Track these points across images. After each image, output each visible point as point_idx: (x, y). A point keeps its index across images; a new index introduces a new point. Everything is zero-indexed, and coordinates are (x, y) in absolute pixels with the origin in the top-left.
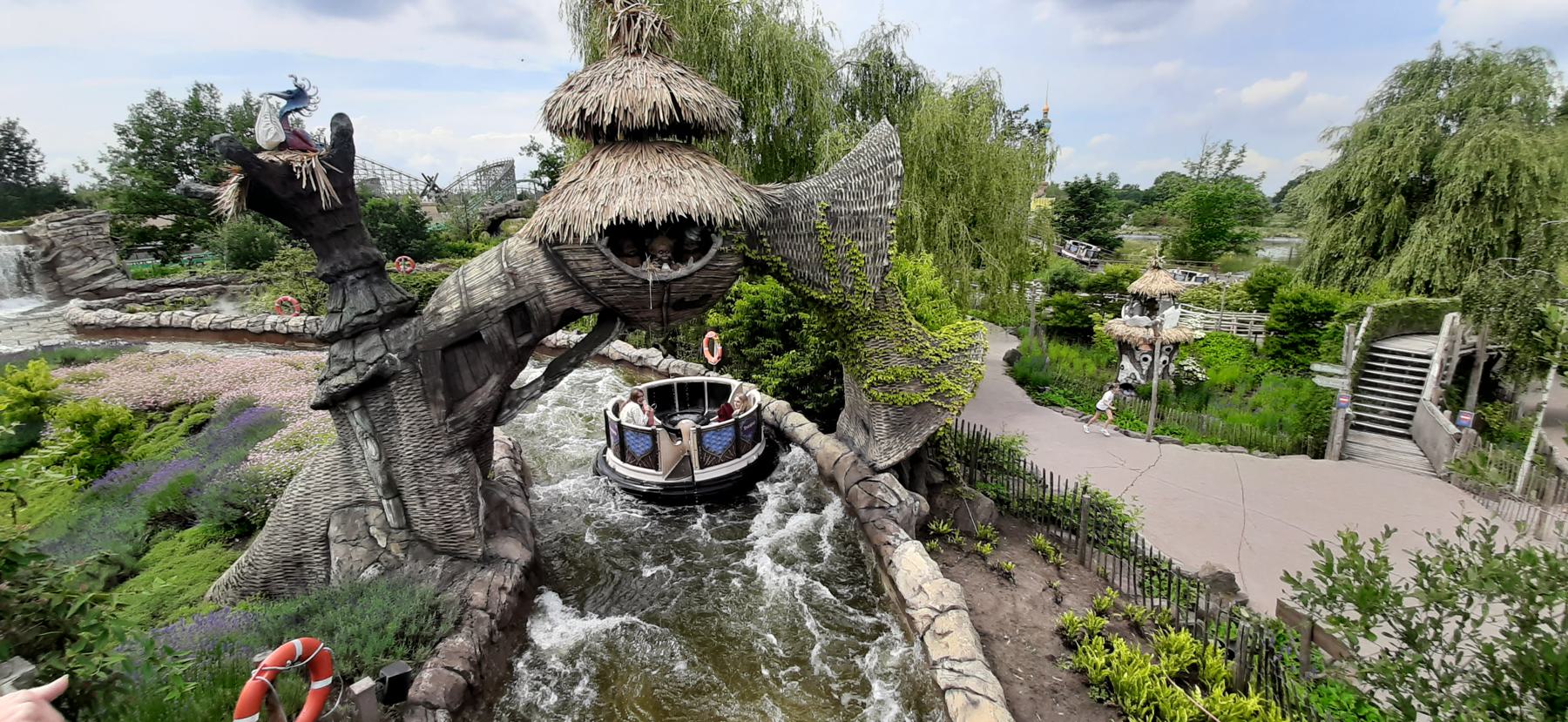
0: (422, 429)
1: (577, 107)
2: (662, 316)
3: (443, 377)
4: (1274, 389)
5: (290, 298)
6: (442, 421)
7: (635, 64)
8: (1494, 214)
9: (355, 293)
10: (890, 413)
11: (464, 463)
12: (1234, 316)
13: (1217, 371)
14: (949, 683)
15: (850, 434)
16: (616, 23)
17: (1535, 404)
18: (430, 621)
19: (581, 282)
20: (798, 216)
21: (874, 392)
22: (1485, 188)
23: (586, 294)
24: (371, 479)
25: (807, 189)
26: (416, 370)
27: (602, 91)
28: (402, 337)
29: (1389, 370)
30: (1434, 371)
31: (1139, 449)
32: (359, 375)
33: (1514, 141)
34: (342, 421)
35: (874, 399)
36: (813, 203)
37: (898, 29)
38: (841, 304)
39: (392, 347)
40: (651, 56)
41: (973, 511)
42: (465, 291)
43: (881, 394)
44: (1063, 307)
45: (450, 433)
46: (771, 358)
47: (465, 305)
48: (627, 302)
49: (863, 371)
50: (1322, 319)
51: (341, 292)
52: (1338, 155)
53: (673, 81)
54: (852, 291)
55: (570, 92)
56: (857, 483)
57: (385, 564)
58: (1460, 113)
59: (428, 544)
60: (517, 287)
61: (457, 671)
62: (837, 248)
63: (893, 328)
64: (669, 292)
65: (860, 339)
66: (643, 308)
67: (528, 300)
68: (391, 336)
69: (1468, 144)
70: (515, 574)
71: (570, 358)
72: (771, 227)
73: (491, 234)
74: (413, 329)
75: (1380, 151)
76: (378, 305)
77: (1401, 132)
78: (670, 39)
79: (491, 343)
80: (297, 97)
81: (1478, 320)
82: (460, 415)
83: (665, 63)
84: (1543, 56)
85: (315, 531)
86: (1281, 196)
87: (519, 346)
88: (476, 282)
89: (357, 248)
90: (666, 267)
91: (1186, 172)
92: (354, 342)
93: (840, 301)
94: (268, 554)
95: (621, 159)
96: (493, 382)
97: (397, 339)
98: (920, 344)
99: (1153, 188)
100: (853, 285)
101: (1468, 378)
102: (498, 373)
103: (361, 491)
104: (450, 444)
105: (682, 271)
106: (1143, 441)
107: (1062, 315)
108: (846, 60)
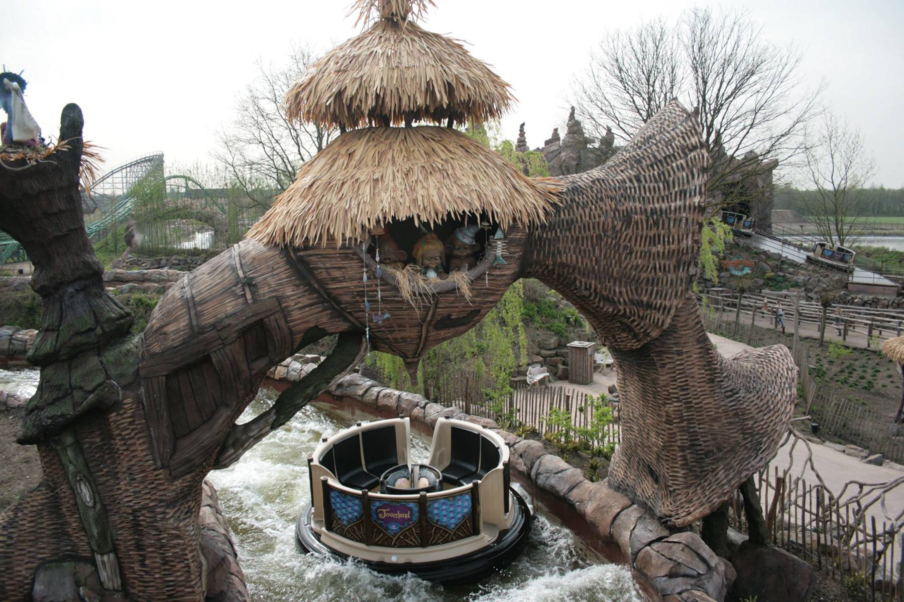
2: (420, 337)
10: (689, 457)
19: (329, 295)
24: (84, 529)
32: (75, 405)
36: (602, 199)
51: (58, 307)
56: (649, 544)
67: (268, 317)
71: (307, 387)
76: (97, 322)
87: (253, 372)
92: (70, 366)
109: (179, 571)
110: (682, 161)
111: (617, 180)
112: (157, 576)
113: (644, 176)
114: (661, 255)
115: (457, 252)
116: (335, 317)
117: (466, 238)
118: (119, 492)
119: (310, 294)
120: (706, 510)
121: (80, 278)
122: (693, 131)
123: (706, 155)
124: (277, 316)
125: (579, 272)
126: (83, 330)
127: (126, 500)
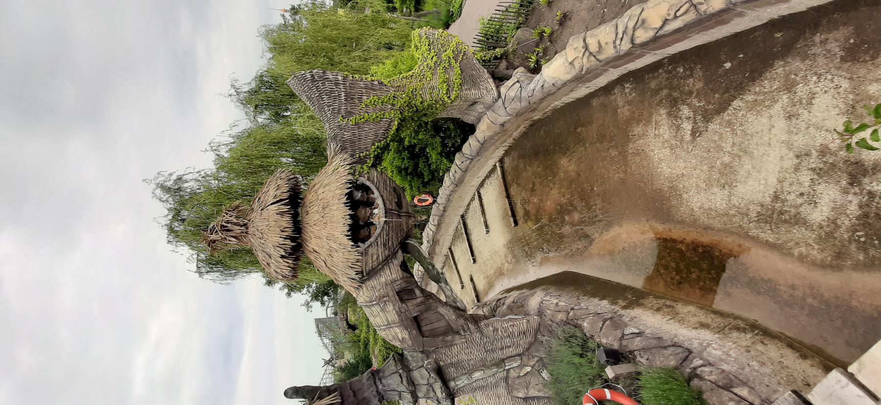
0: (467, 347)
1: (280, 260)
2: (406, 216)
6: (463, 337)
7: (253, 227)
9: (389, 385)
10: (466, 87)
11: (487, 326)
14: (629, 40)
15: (477, 114)
16: (228, 238)
18: (574, 341)
19: (385, 260)
20: (347, 135)
21: (452, 97)
23: (391, 258)
25: (331, 129)
26: (434, 351)
27: (270, 245)
28: (415, 359)
34: (461, 390)
35: (457, 97)
36: (340, 126)
37: (233, 86)
38: (401, 112)
39: (421, 364)
40: (248, 218)
41: (524, 42)
42: (389, 325)
43: (454, 92)
46: (431, 164)
47: (397, 325)
48: (397, 235)
49: (441, 103)
54: (393, 105)
55: (271, 265)
57: (541, 367)
59: (531, 345)
60: (388, 296)
61: (603, 325)
62: (367, 112)
63: (415, 84)
65: (421, 103)
66: (400, 226)
67: (395, 290)
68: (414, 365)
72: (354, 151)
74: (411, 353)
76: (396, 372)
78: (237, 207)
79: (420, 311)
83: (252, 209)
87: (422, 295)
88: (384, 319)
89: (363, 384)
90: (376, 211)
92: (417, 385)
93: (399, 113)
96: (442, 310)
97: (416, 362)
98: (426, 68)
100: (389, 104)
102: (437, 307)
103: (500, 380)
104: (476, 333)
105: (379, 201)
108: (252, 119)
109: (513, 330)
110: (320, 83)
111: (330, 117)
112: (515, 340)
113: (328, 103)
114: (368, 97)
115: (365, 200)
116: (396, 256)
117: (358, 195)
118: (477, 358)
119: (384, 269)
120: (491, 81)
122: (304, 76)
124: (394, 285)
125: (376, 138)
126: (400, 380)
127: (480, 355)
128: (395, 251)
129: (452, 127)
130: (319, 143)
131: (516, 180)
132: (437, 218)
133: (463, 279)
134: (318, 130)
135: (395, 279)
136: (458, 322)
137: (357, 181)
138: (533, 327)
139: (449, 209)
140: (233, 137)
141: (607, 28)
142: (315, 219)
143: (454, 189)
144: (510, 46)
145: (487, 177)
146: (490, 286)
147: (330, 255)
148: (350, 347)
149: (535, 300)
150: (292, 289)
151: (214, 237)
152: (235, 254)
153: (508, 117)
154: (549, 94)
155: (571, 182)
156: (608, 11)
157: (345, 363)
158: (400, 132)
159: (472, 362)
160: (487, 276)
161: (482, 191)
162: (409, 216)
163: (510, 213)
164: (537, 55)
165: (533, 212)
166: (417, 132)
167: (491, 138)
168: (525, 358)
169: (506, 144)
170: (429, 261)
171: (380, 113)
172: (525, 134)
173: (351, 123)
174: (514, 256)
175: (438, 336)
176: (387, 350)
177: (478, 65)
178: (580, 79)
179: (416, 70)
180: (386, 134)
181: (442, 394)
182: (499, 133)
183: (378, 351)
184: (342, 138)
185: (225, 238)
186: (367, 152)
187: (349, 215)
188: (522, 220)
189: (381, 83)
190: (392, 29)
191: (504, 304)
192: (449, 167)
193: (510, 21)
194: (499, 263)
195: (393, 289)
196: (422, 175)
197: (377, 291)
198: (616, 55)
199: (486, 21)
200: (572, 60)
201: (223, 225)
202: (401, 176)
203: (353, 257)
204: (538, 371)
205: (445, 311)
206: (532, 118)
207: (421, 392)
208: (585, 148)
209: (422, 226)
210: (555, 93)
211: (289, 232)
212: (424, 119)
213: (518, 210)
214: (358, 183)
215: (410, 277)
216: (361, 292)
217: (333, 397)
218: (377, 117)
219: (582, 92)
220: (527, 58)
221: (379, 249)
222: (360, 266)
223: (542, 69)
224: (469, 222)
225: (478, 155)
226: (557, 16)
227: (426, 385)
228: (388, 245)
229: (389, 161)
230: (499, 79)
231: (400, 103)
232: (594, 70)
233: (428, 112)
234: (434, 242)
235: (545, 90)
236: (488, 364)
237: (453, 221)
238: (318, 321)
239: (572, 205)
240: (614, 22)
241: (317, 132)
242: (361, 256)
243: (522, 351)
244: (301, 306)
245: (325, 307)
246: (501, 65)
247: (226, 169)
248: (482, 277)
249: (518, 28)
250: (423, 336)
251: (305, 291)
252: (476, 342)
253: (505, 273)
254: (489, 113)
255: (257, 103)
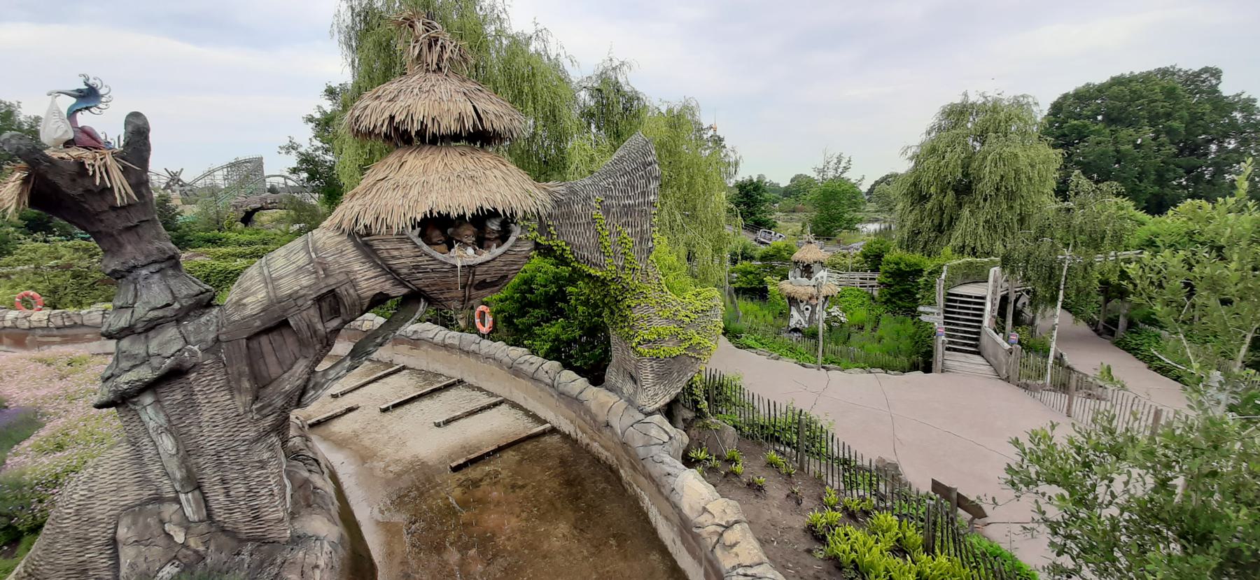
1: (387, 115)
2: (464, 296)
3: (248, 365)
4: (890, 325)
5: (32, 293)
8: (1007, 202)
9: (148, 287)
10: (655, 365)
11: (271, 448)
12: (858, 275)
13: (852, 314)
15: (620, 386)
17: (1051, 326)
19: (390, 269)
20: (578, 208)
21: (639, 349)
22: (1001, 186)
25: (584, 186)
27: (410, 101)
29: (960, 308)
30: (988, 307)
31: (815, 376)
32: (154, 369)
33: (1016, 155)
35: (641, 355)
36: (590, 198)
37: (623, 64)
38: (614, 279)
39: (192, 339)
40: (451, 74)
42: (270, 281)
43: (647, 350)
44: (745, 273)
45: (257, 420)
46: (541, 326)
48: (433, 285)
49: (631, 333)
50: (914, 275)
51: (132, 287)
52: (912, 164)
53: (474, 96)
54: (623, 268)
55: (377, 102)
57: (184, 561)
58: (982, 136)
59: (232, 534)
60: (327, 276)
62: (610, 234)
63: (653, 295)
64: (474, 275)
65: (629, 306)
67: (338, 287)
69: (989, 158)
70: (325, 550)
72: (556, 218)
73: (246, 225)
75: (938, 162)
76: (175, 298)
77: (949, 149)
78: (465, 60)
80: (88, 96)
81: (1012, 272)
82: (267, 401)
84: (1030, 100)
85: (99, 534)
86: (870, 191)
87: (328, 330)
88: (282, 272)
89: (151, 243)
90: (470, 251)
91: (814, 175)
92: (147, 337)
93: (613, 276)
94: (48, 563)
95: (428, 160)
96: (300, 367)
99: (789, 186)
100: (624, 263)
101: (1005, 310)
104: (255, 431)
105: (486, 256)
106: (815, 370)
107: (744, 279)
108: (584, 84)
109: (263, 495)
120: (667, 399)
121: (155, 262)
123: (658, 168)
128: (407, 283)
129: (598, 351)
130: (558, 168)
131: (526, 457)
132: (456, 342)
133: (350, 394)
134: (577, 168)
135: (358, 285)
136: (278, 397)
137: (515, 224)
138: (269, 532)
139: (472, 360)
140: (556, 59)
141: (756, 551)
142: (455, 165)
143: (506, 364)
144: (713, 420)
145: (527, 412)
146: (340, 444)
147: (397, 186)
148: (207, 213)
149: (322, 527)
150: (324, 125)
151: (419, 26)
152: (386, 48)
153: (619, 431)
154: (658, 485)
155: (532, 547)
156: (775, 547)
157: (177, 207)
158: (586, 280)
159: (195, 430)
160: (358, 436)
161: (504, 407)
162: (464, 301)
163: (472, 456)
164: (706, 459)
165: (479, 493)
166: (586, 303)
167: (587, 411)
168: (203, 527)
169: (580, 434)
170: (391, 336)
171: (610, 251)
172: (596, 460)
173: (594, 213)
174: (399, 475)
175: (251, 365)
176: (205, 277)
177: (685, 380)
178: (686, 528)
179: (671, 296)
180: (582, 261)
181: (127, 383)
182: (595, 421)
183: (203, 262)
184: (574, 201)
185: (417, 42)
186: (555, 236)
187: (464, 213)
188: (463, 478)
189: (650, 251)
190: (713, 260)
191: (310, 471)
192: (537, 353)
193: (742, 415)
194: (383, 452)
195: (342, 283)
196: (523, 316)
197: (334, 258)
198: (724, 571)
199: (738, 383)
200: (710, 510)
201: (438, 40)
202: (519, 285)
203: (395, 219)
204: (175, 558)
205: (301, 370)
206: (621, 466)
207: (131, 345)
208: (587, 557)
209: (447, 322)
210: (662, 494)
211: (432, 129)
212: (606, 312)
213: (478, 469)
214: (512, 225)
215: (362, 310)
216: (332, 234)
217: (126, 193)
218: (606, 248)
219: (667, 533)
220: (700, 446)
221: (411, 259)
222: (380, 231)
223: (692, 470)
224: (452, 393)
225: (561, 394)
226: (759, 478)
227: (147, 353)
228: (416, 272)
229: (543, 267)
230: (669, 411)
231: (627, 277)
232: (699, 544)
233: (616, 315)
234: (415, 342)
235: (665, 479)
236: (192, 460)
237: (451, 368)
238: (258, 164)
239: (495, 556)
240: (765, 559)
241: (573, 167)
242: (398, 232)
243: (218, 519)
244: (290, 137)
245: (287, 174)
246: (687, 411)
247: (514, 47)
248: (356, 426)
249: (735, 427)
250: (248, 339)
251: (318, 143)
252: (237, 433)
253: (366, 465)
254: (622, 404)
255: (604, 92)
